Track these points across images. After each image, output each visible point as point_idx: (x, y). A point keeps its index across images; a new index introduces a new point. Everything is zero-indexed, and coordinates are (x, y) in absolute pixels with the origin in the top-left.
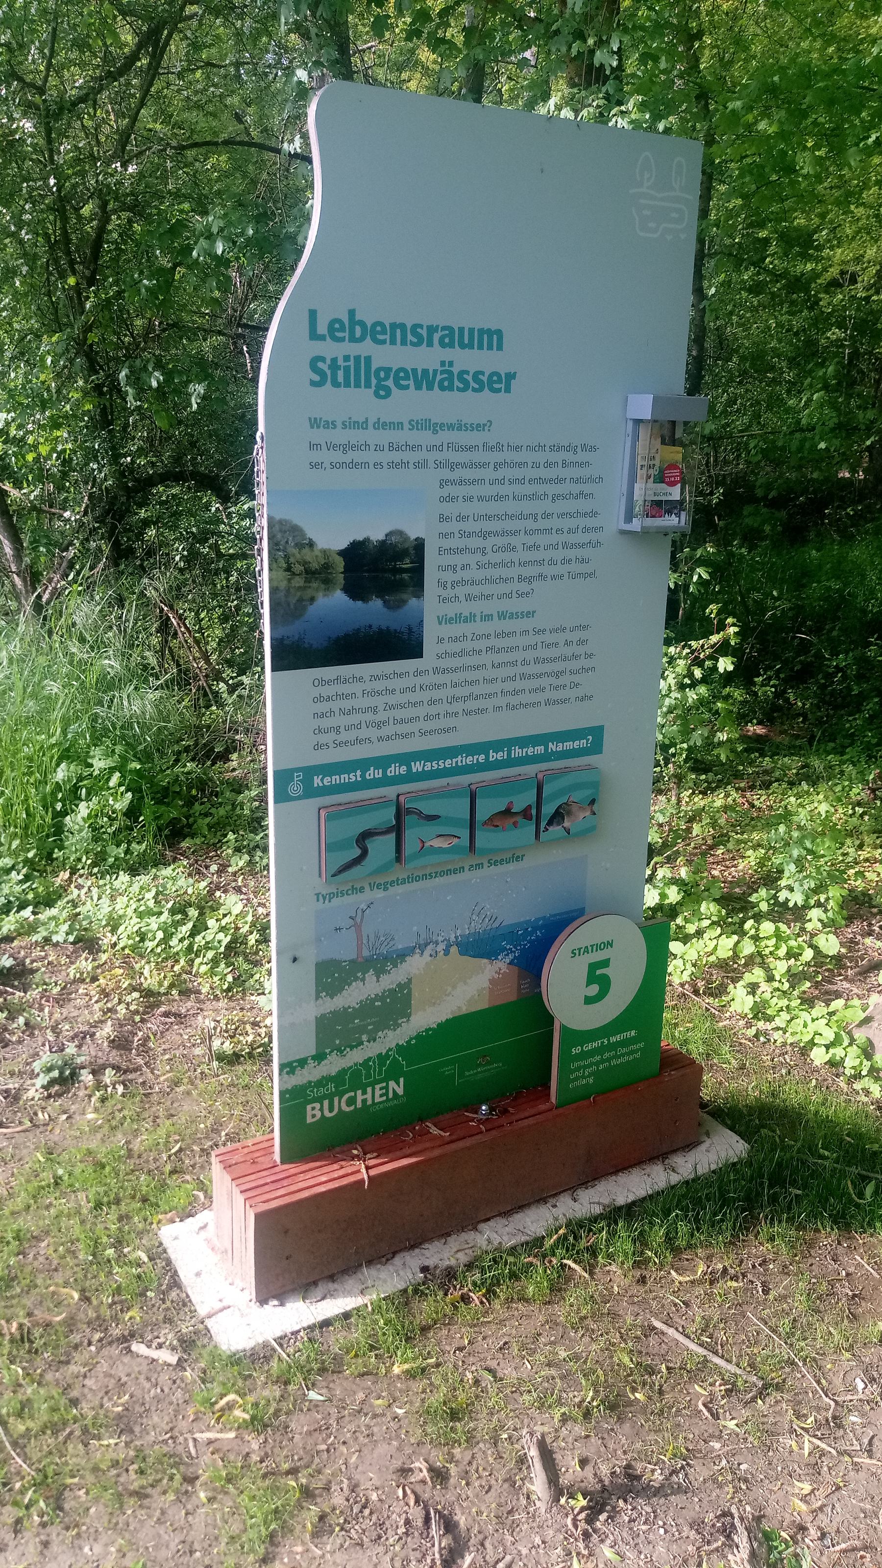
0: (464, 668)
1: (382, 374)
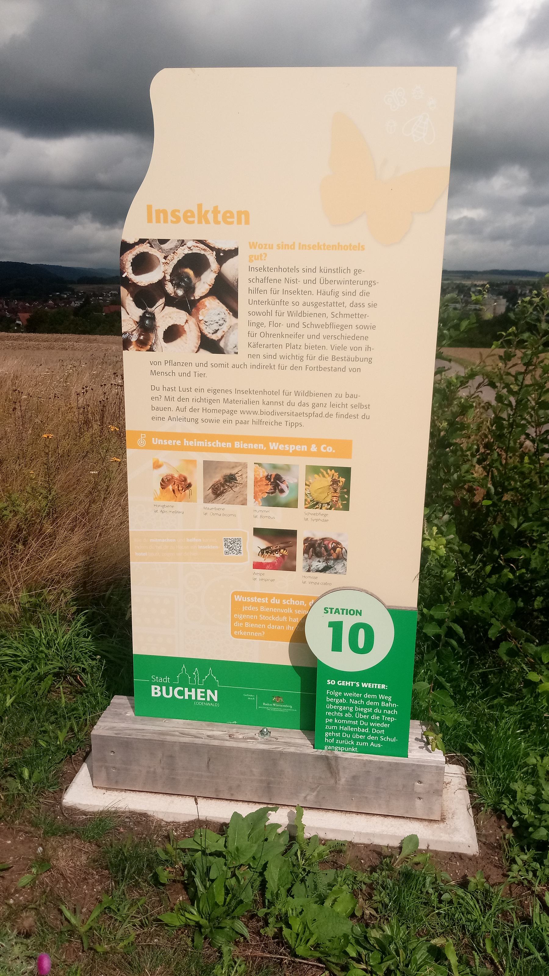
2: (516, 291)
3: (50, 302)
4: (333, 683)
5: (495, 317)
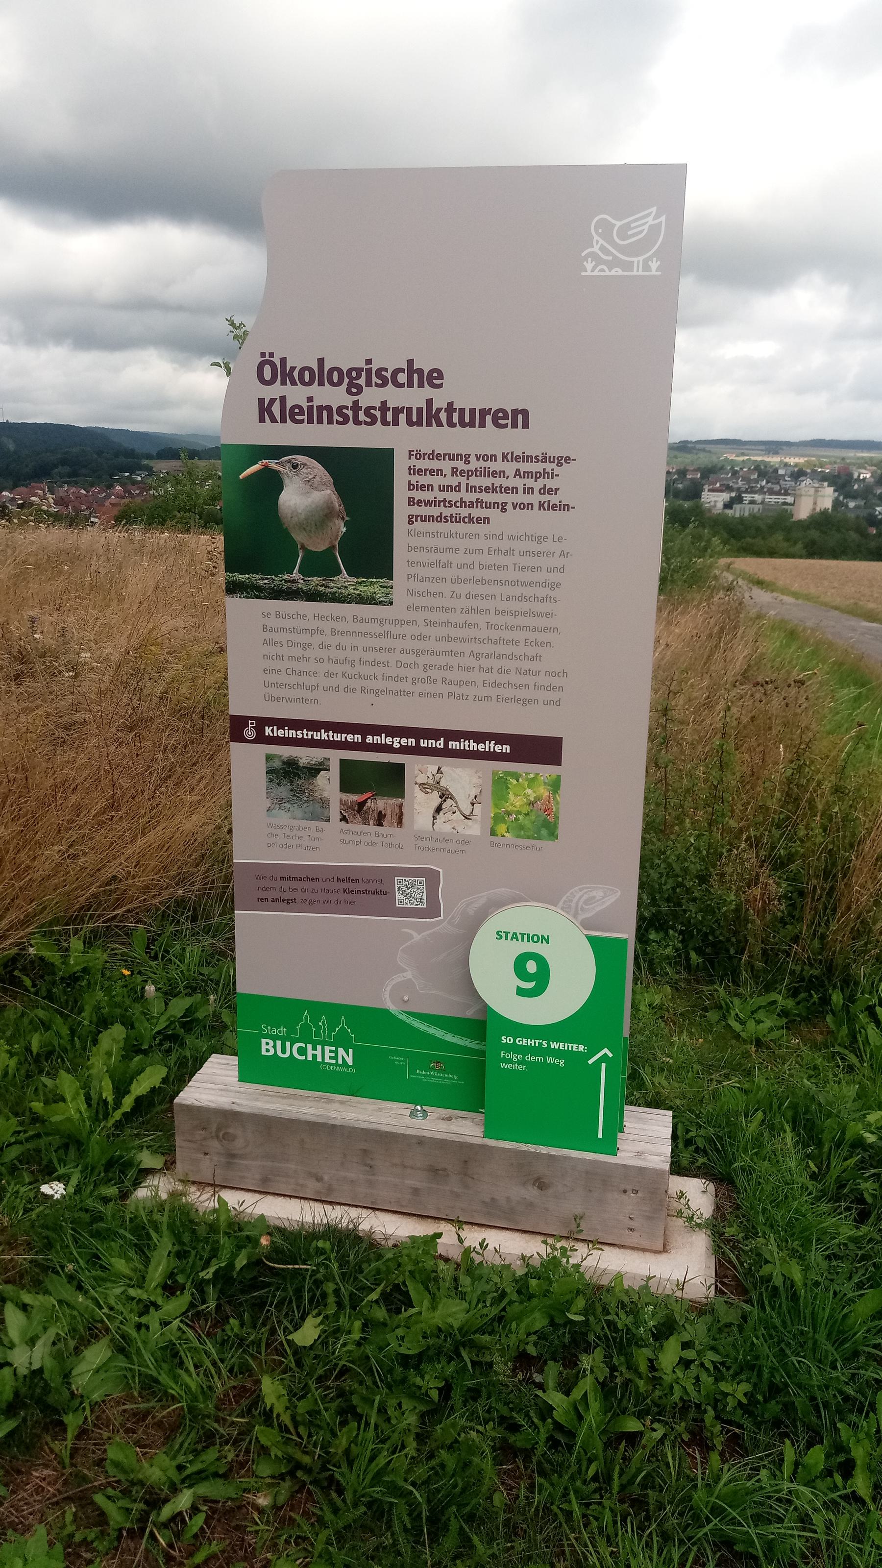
0: (515, 614)
1: (354, 374)
2: (850, 475)
3: (118, 488)
4: (509, 1040)
5: (812, 517)
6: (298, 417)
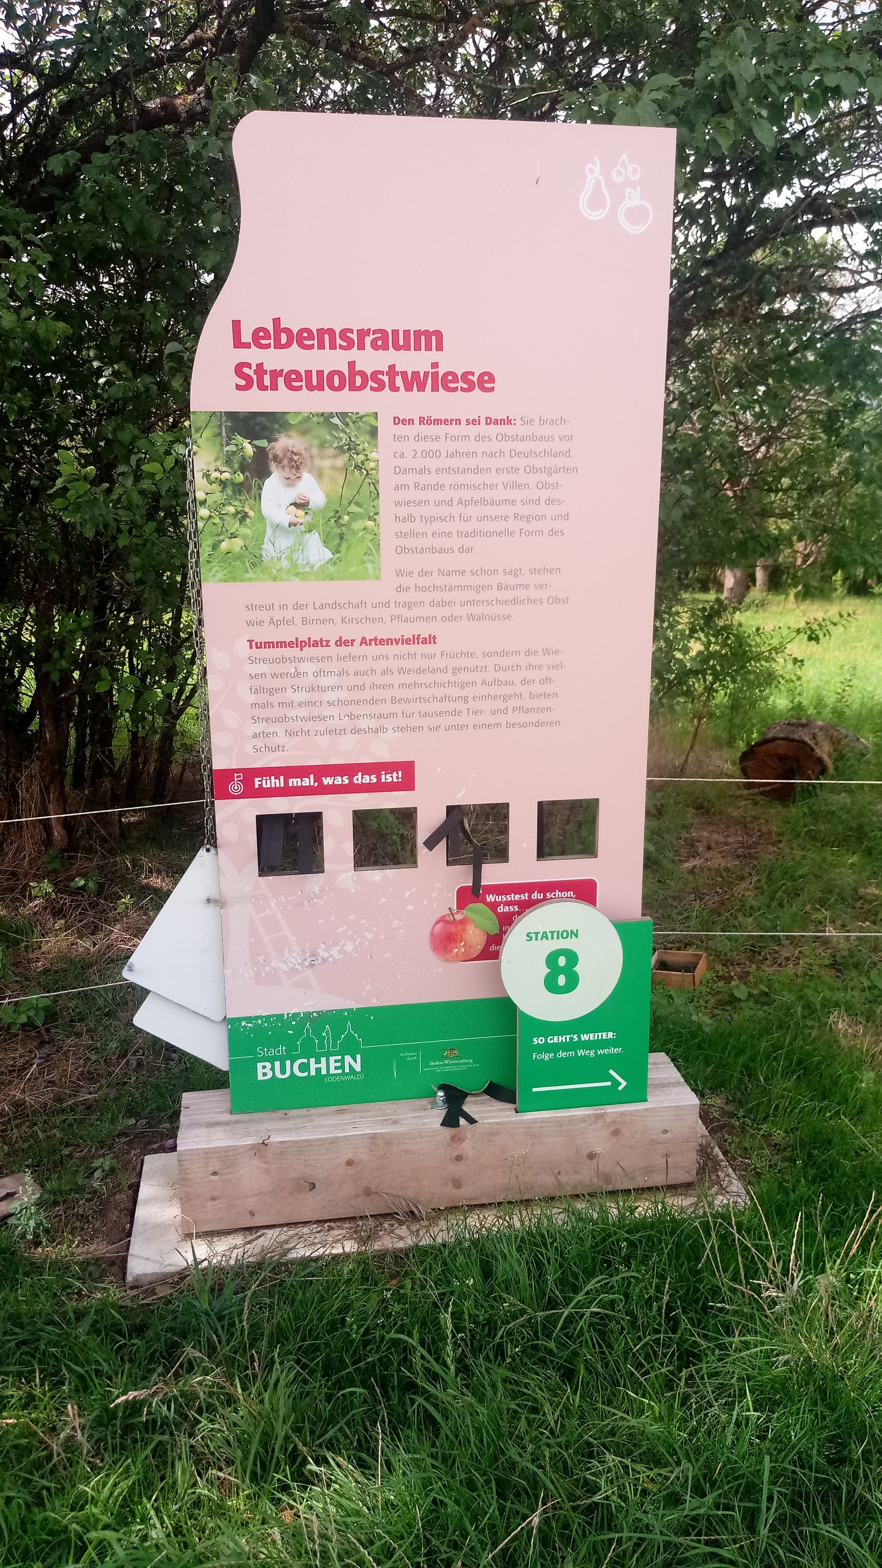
6: (451, 385)
